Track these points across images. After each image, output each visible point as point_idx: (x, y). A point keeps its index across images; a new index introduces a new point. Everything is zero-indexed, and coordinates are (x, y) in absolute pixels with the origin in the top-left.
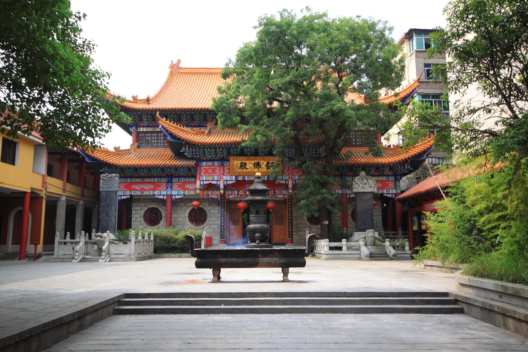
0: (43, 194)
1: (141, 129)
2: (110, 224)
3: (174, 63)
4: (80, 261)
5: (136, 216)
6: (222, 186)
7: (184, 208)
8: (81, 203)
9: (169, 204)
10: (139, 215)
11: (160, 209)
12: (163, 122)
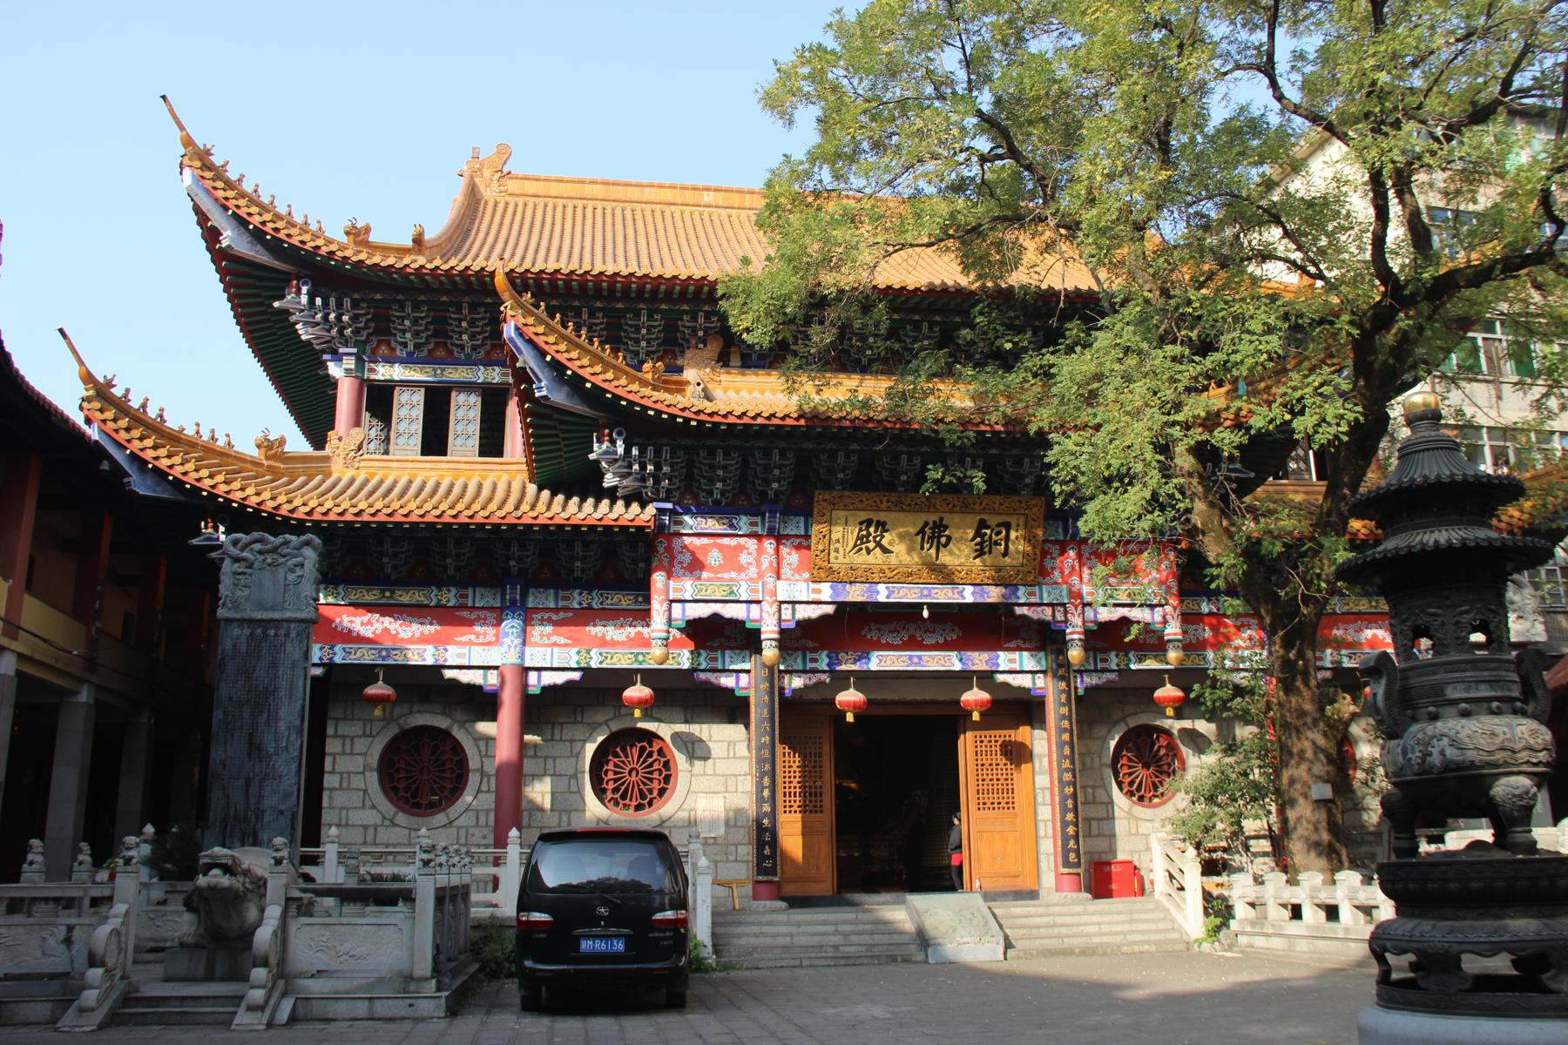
4: (113, 1020)
5: (344, 764)
6: (769, 631)
7: (569, 732)
8: (84, 696)
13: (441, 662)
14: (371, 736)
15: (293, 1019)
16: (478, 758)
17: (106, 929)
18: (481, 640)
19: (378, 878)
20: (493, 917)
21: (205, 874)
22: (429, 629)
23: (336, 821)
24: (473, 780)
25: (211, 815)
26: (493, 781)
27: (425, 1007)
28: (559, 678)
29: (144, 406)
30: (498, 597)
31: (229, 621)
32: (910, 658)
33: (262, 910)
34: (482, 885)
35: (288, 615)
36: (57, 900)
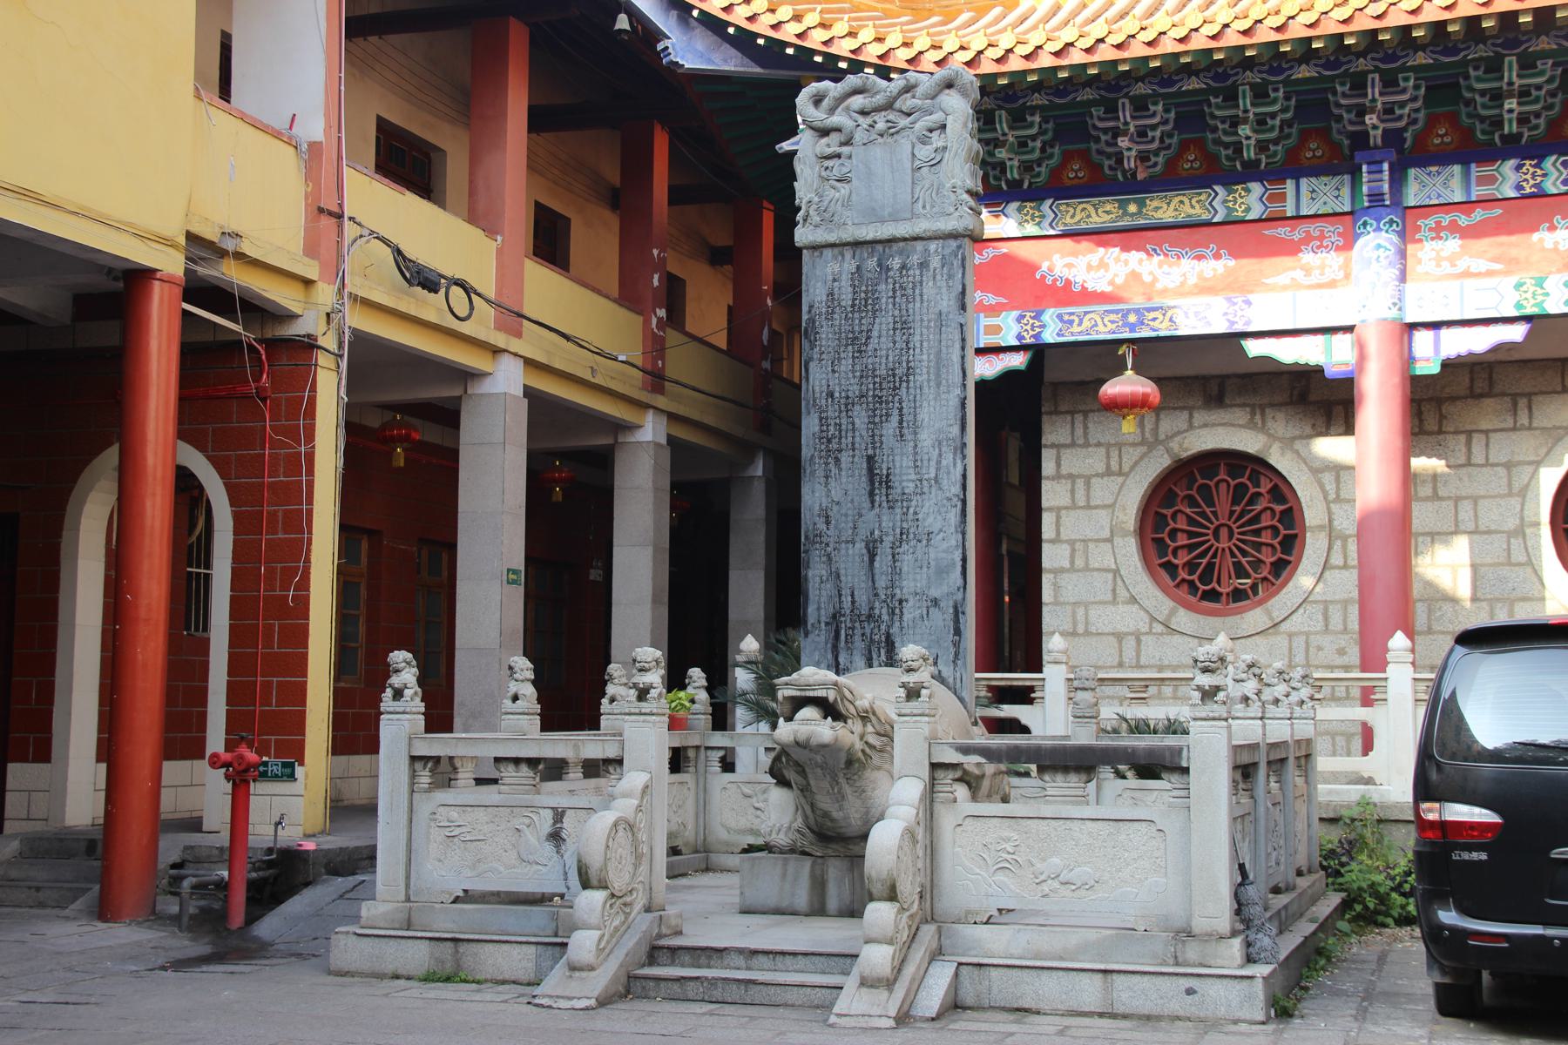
0: (311, 315)
2: (910, 584)
4: (630, 988)
7: (1503, 447)
8: (651, 430)
13: (1239, 328)
14: (1120, 474)
15: (954, 1006)
16: (1322, 506)
17: (606, 818)
18: (1315, 279)
19: (1140, 727)
20: (1365, 803)
21: (789, 719)
22: (1216, 267)
23: (1068, 627)
24: (1314, 547)
25: (811, 609)
26: (1352, 547)
27: (1222, 998)
28: (1478, 341)
30: (1346, 192)
31: (815, 248)
34: (1340, 741)
35: (921, 227)
36: (532, 762)
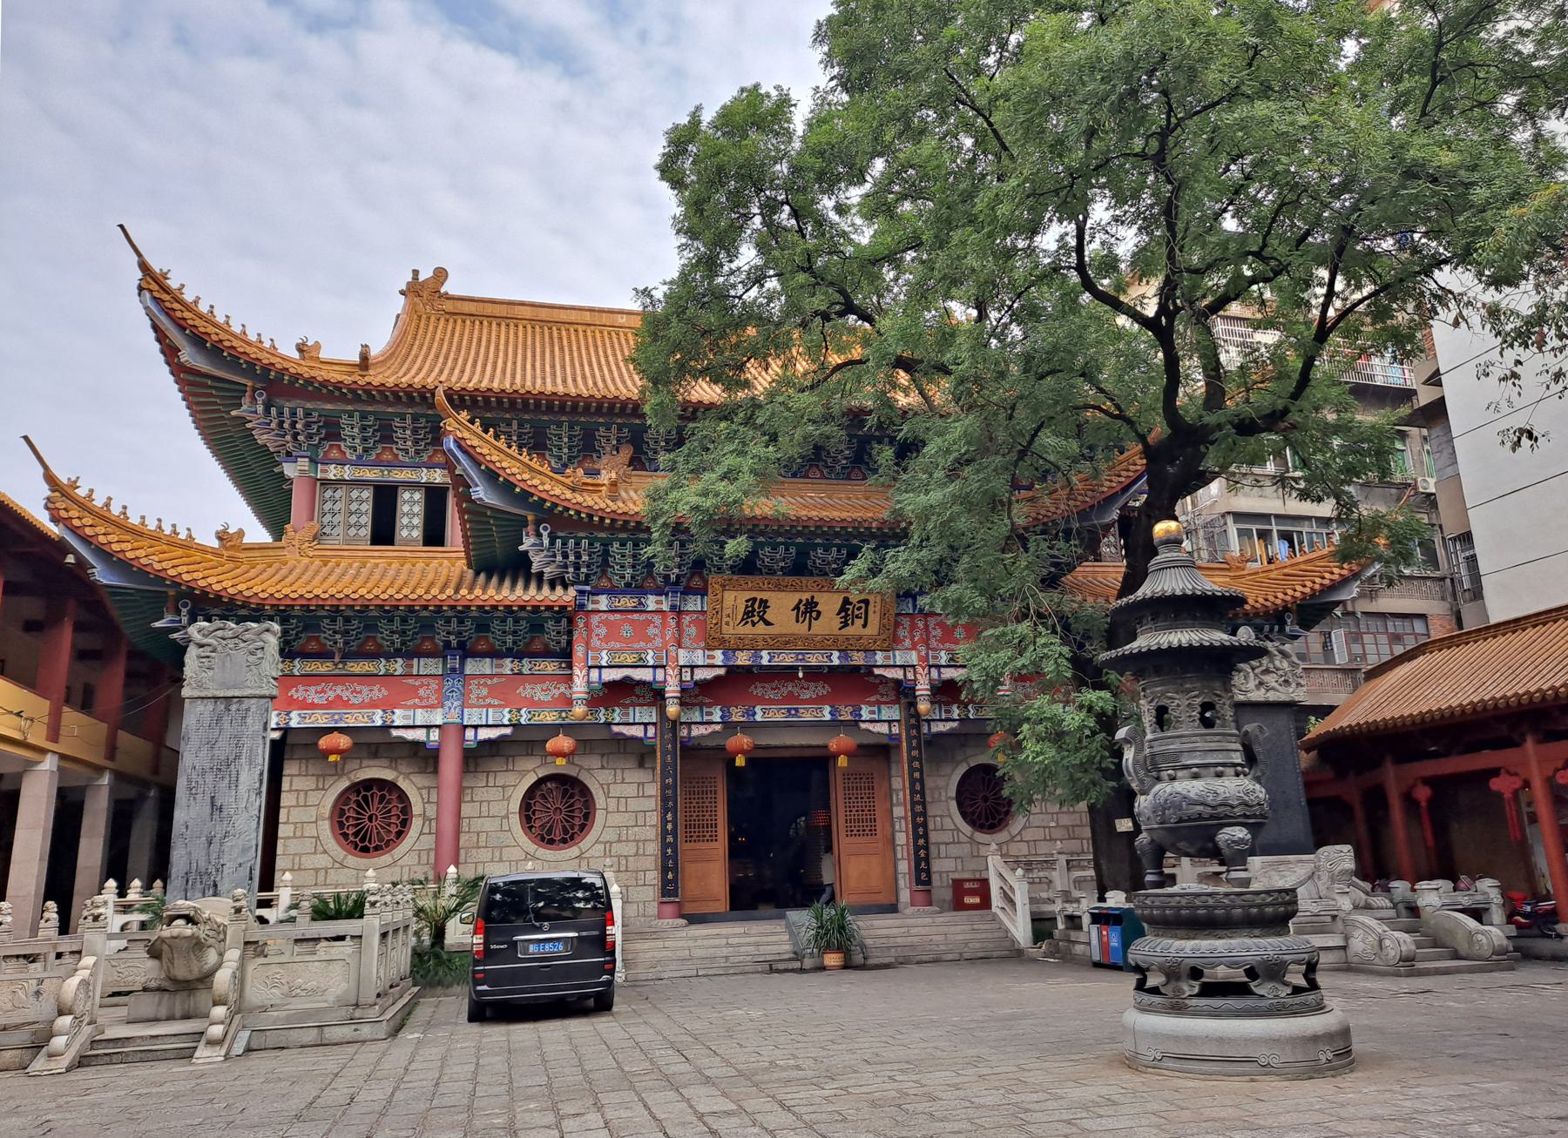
1: (333, 472)
3: (421, 278)
4: (82, 1062)
7: (501, 780)
9: (450, 763)
10: (313, 811)
11: (403, 784)
12: (459, 427)
17: (74, 982)
28: (493, 734)
29: (107, 505)
32: (789, 710)
33: (221, 955)
36: (25, 957)
